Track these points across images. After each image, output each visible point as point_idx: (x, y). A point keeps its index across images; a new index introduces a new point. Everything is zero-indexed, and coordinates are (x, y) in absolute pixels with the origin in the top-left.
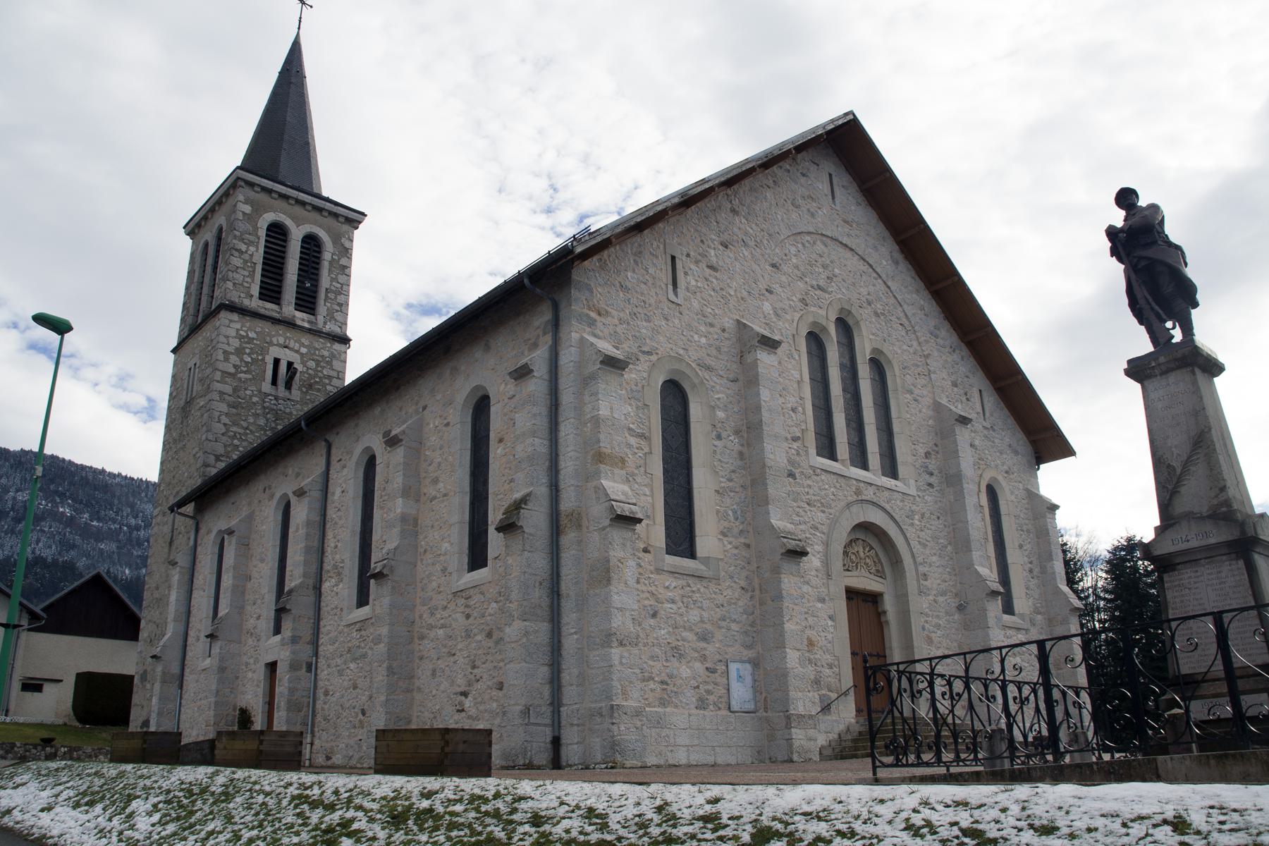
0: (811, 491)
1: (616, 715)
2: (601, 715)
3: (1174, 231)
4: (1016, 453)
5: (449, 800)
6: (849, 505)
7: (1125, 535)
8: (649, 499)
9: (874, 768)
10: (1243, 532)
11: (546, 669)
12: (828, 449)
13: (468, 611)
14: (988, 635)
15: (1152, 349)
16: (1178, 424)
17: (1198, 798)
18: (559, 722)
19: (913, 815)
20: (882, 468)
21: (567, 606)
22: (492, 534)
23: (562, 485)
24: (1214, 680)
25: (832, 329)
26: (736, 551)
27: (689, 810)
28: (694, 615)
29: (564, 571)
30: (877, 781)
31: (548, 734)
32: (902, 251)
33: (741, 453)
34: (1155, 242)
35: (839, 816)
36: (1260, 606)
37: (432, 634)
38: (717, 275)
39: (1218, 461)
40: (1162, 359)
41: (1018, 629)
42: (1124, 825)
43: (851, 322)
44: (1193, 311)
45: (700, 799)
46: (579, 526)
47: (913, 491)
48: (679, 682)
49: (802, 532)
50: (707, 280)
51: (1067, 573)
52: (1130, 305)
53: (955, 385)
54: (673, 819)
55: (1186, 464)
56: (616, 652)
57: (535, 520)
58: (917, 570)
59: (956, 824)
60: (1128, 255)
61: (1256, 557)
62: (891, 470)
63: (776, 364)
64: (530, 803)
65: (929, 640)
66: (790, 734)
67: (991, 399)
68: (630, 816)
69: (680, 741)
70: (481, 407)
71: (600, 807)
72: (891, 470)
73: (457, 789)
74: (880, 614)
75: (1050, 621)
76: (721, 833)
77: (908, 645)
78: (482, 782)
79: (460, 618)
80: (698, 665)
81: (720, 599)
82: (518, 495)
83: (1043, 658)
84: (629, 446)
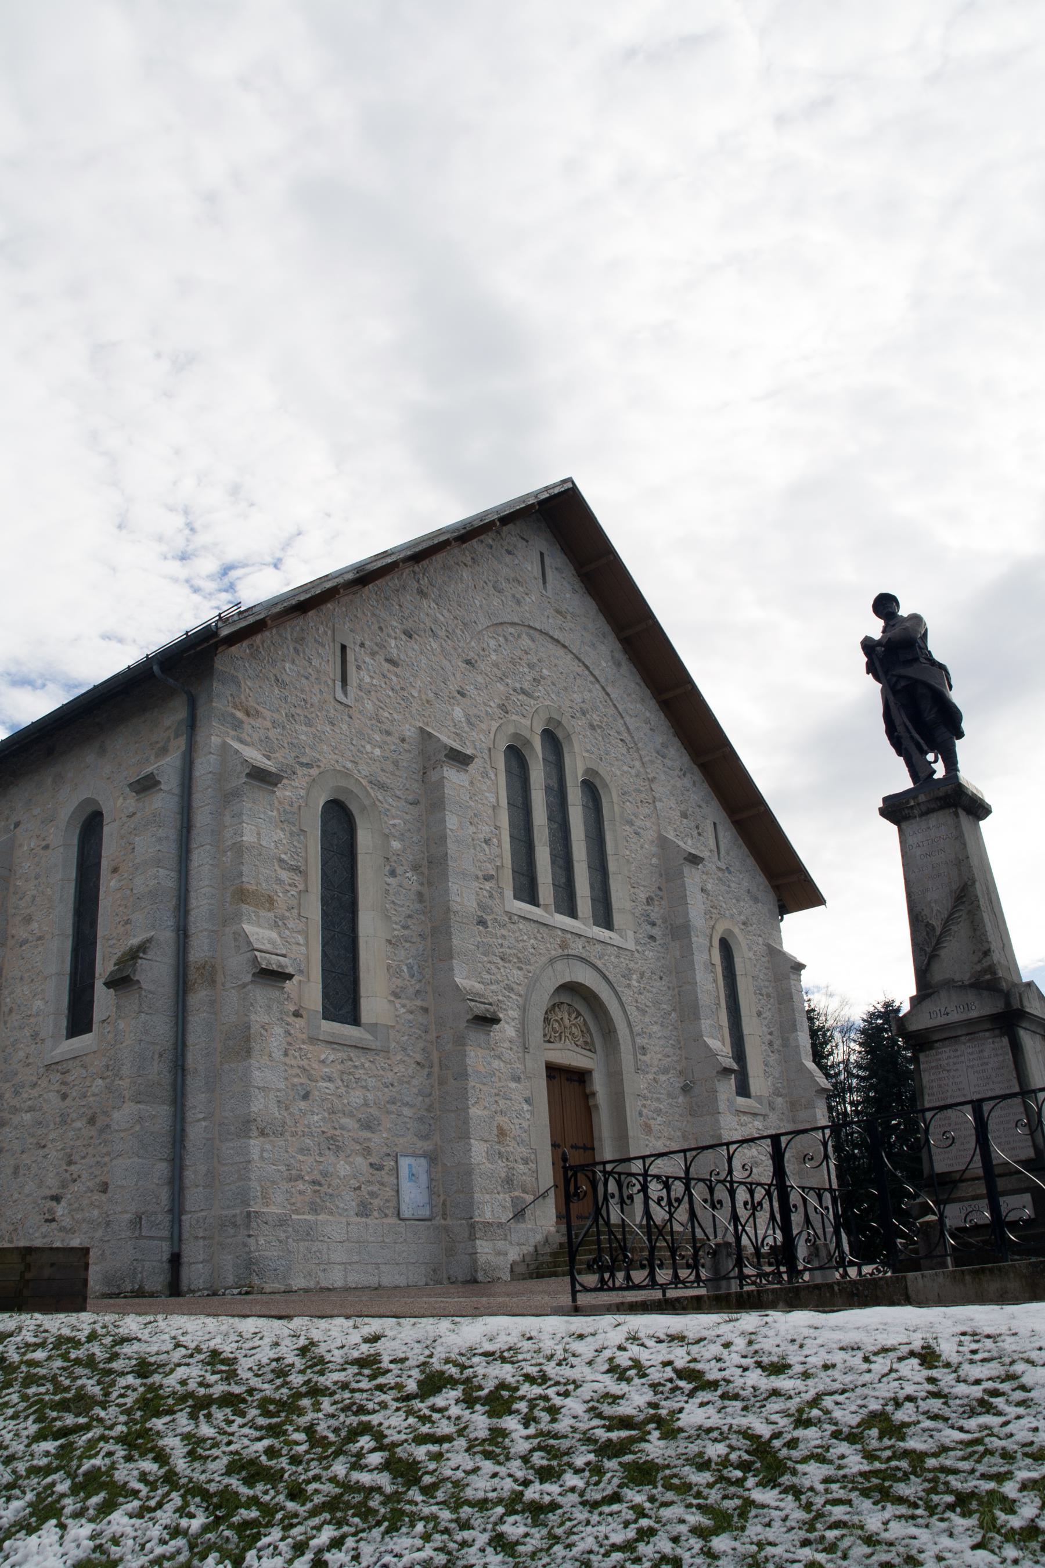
0: (506, 943)
1: (254, 1224)
2: (234, 1225)
3: (938, 647)
4: (756, 900)
5: (27, 1345)
6: (552, 961)
7: (882, 999)
8: (303, 949)
9: (574, 1293)
10: (1008, 1004)
12: (528, 891)
13: (64, 1089)
14: (717, 1121)
15: (907, 784)
16: (939, 875)
17: (949, 1323)
19: (619, 1353)
20: (594, 916)
21: (195, 1084)
23: (192, 929)
24: (973, 1179)
25: (537, 743)
26: (411, 1017)
27: (341, 1352)
28: (356, 1097)
29: (191, 1039)
30: (576, 1310)
31: (164, 1250)
33: (420, 895)
34: (916, 660)
35: (528, 1356)
36: (1026, 1092)
37: (16, 1119)
38: (398, 670)
39: (983, 921)
40: (922, 798)
41: (755, 1115)
42: (866, 1360)
43: (560, 735)
44: (957, 742)
45: (355, 1337)
46: (213, 982)
47: (631, 945)
48: (336, 1182)
50: (384, 676)
51: (814, 1046)
53: (684, 815)
54: (320, 1364)
56: (255, 1144)
57: (156, 973)
58: (634, 1042)
59: (670, 1363)
60: (886, 673)
61: (1022, 1033)
62: (605, 917)
63: (466, 784)
64: (136, 1346)
65: (648, 1129)
66: (474, 1247)
67: (728, 835)
68: (265, 1361)
69: (334, 1257)
70: (91, 825)
71: (227, 1349)
72: (605, 917)
73: (39, 1330)
74: (587, 1097)
75: (793, 1105)
76: (381, 1380)
77: (622, 1136)
78: (73, 1318)
79: (54, 1098)
80: (359, 1160)
81: (389, 1076)
82: (135, 941)
83: (778, 1157)
84: (279, 881)
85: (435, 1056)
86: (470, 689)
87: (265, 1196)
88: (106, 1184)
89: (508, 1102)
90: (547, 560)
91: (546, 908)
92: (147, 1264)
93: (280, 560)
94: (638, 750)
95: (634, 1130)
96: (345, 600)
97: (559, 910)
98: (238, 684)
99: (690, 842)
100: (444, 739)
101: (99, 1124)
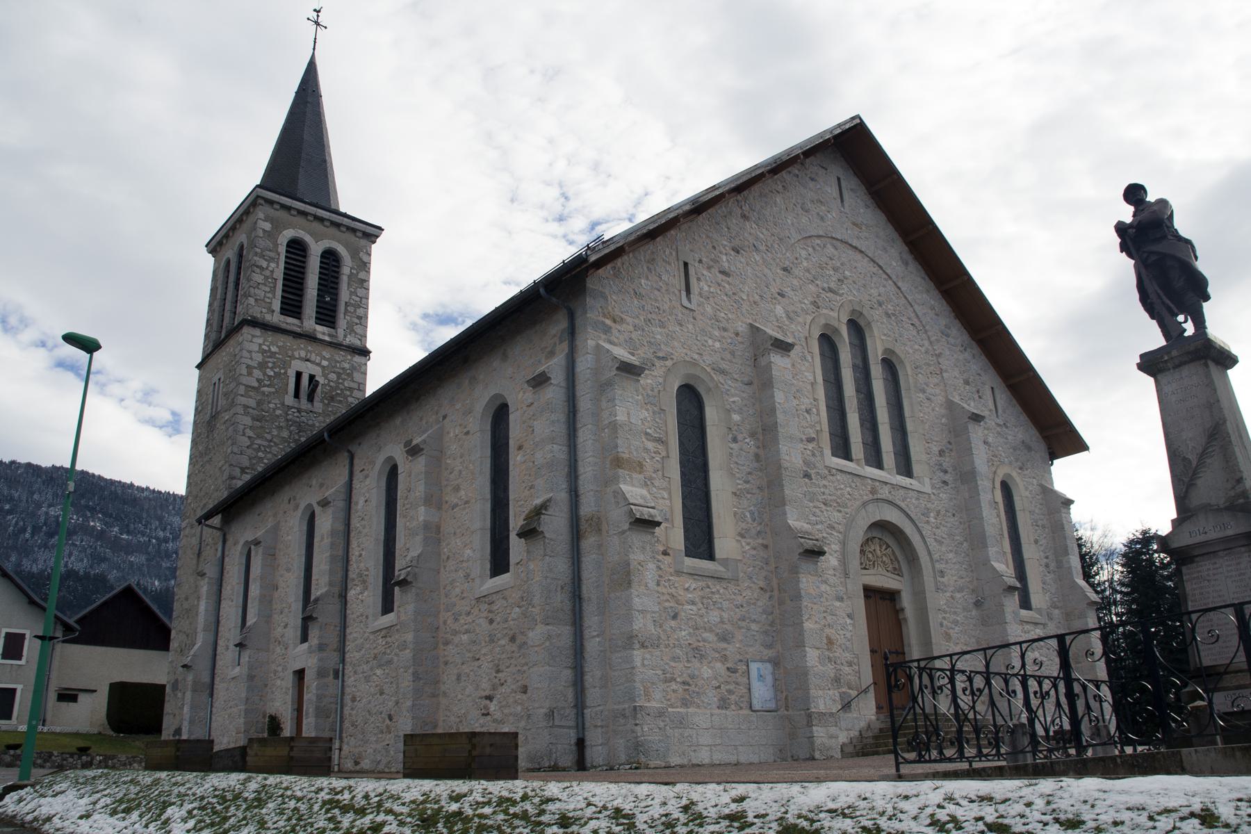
0: (827, 491)
1: (639, 716)
2: (624, 716)
3: (1182, 225)
5: (477, 803)
6: (864, 504)
7: (1140, 528)
12: (842, 448)
13: (491, 616)
14: (1005, 630)
15: (1162, 342)
17: (1225, 790)
18: (583, 724)
19: (938, 810)
20: (897, 467)
21: (589, 610)
23: (581, 490)
26: (754, 552)
28: (714, 616)
29: (585, 575)
30: (900, 778)
31: (572, 736)
32: (911, 252)
33: (757, 456)
34: (1164, 237)
35: (864, 813)
37: (456, 639)
38: (730, 279)
39: (1234, 453)
40: (1174, 353)
41: (1036, 624)
42: (1151, 818)
43: (862, 323)
44: (1205, 305)
45: (726, 798)
51: (1083, 567)
53: (967, 382)
55: (1203, 455)
57: (555, 525)
58: (933, 567)
59: (981, 819)
62: (906, 468)
63: (789, 366)
64: (558, 805)
65: (948, 637)
66: (811, 732)
67: (1003, 397)
68: (656, 816)
69: (702, 741)
70: (500, 415)
71: (627, 807)
72: (906, 468)
73: (485, 792)
74: (898, 612)
75: (1068, 616)
77: (927, 641)
78: (509, 784)
79: (484, 623)
80: (719, 665)
82: (538, 501)
83: (1063, 652)
84: (646, 450)
85: (775, 583)
86: (788, 290)
87: (647, 694)
90: (843, 184)
92: (559, 747)
94: (926, 332)
96: (685, 227)
97: (868, 464)
98: (605, 298)
100: (770, 331)
101: (518, 642)
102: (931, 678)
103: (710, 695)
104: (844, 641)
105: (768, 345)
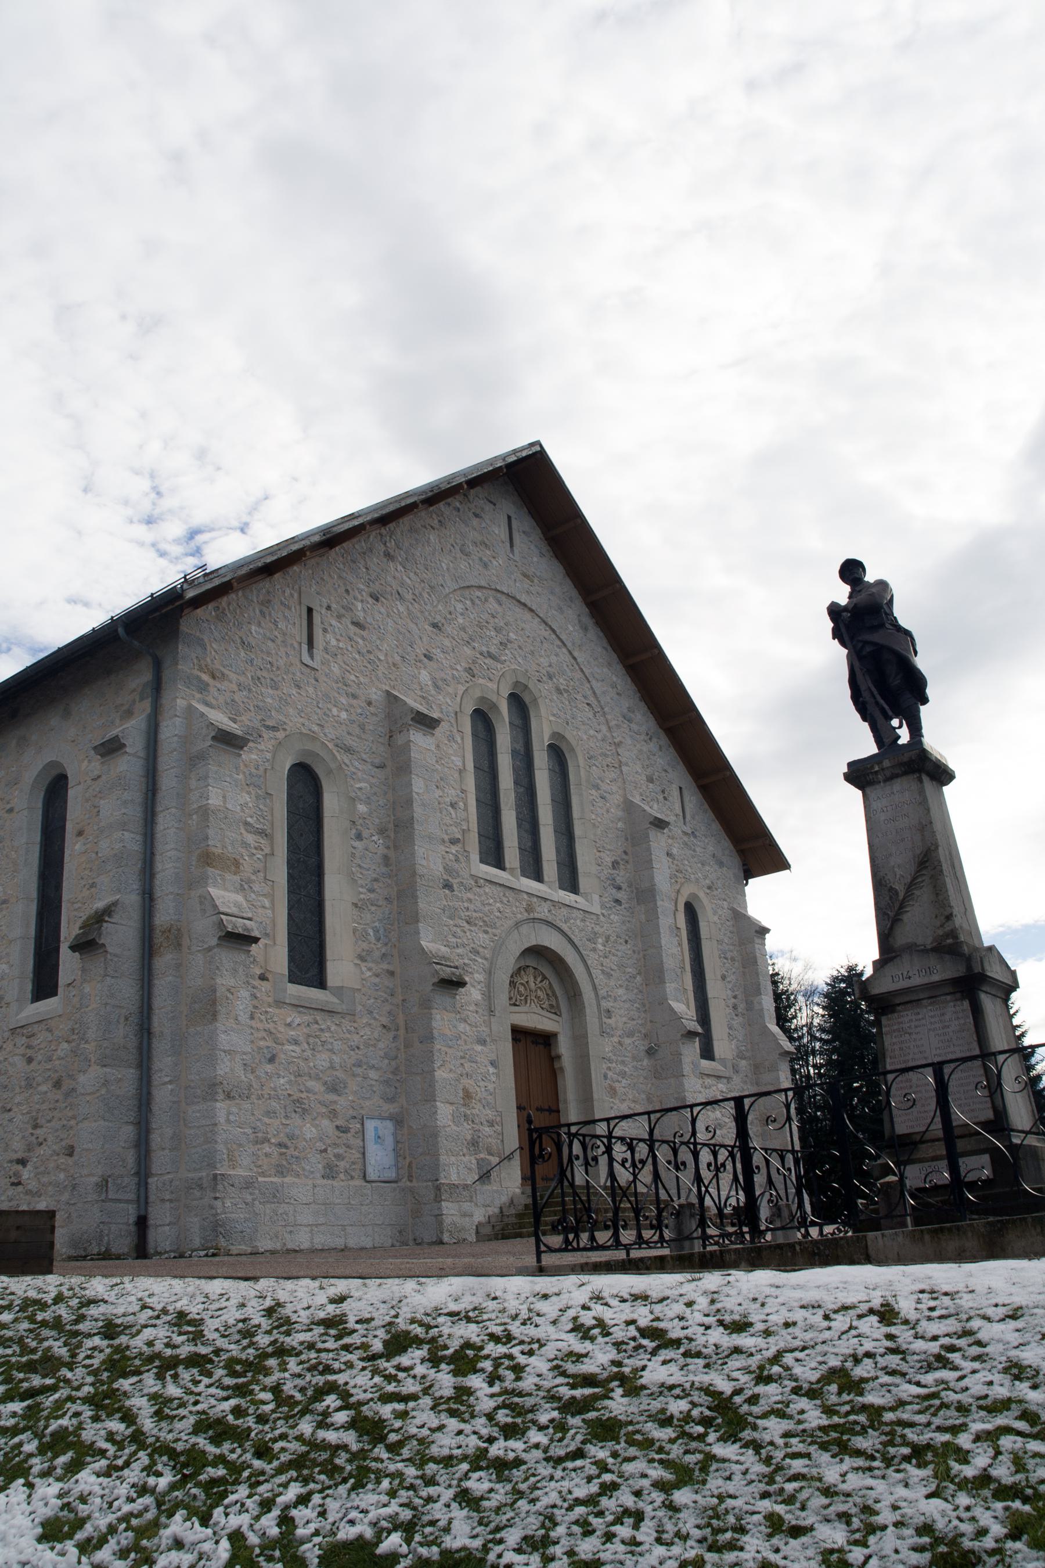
0: (472, 907)
1: (220, 1187)
2: (201, 1187)
3: (904, 613)
4: (721, 864)
6: (517, 925)
7: (846, 963)
9: (539, 1254)
10: (969, 968)
11: (130, 1128)
12: (494, 855)
13: (29, 1052)
14: (682, 1084)
15: (875, 750)
17: (908, 1281)
18: (147, 1198)
19: (583, 1312)
20: (560, 879)
21: (161, 1049)
22: (65, 953)
23: (158, 893)
25: (504, 707)
26: (377, 980)
27: (307, 1312)
28: (322, 1060)
29: (157, 1002)
30: (541, 1271)
31: (131, 1213)
32: (593, 615)
33: (386, 858)
34: (882, 625)
35: (493, 1316)
39: (944, 884)
40: (886, 763)
41: (719, 1077)
42: (826, 1317)
43: (527, 699)
44: (922, 708)
45: (321, 1298)
47: (596, 909)
49: (459, 956)
50: (351, 639)
52: (852, 697)
53: (650, 780)
54: (286, 1325)
55: (911, 886)
56: (221, 1107)
57: (121, 936)
58: (599, 1005)
59: (633, 1322)
60: (852, 639)
62: (570, 881)
63: (433, 748)
64: (103, 1308)
65: (613, 1091)
66: (440, 1208)
67: (693, 799)
68: (231, 1322)
70: (56, 789)
71: (194, 1310)
72: (570, 881)
74: (553, 1059)
76: (347, 1340)
78: (39, 1281)
79: (19, 1062)
80: (325, 1122)
82: (100, 905)
83: (741, 1119)
84: (245, 845)
86: (437, 653)
88: (72, 1147)
89: (473, 1065)
90: (515, 524)
91: (512, 871)
92: (113, 1227)
93: (247, 524)
95: (599, 1092)
97: (524, 875)
99: (655, 806)
100: (410, 702)
102: (584, 1145)
103: (313, 1160)
104: (485, 1094)
105: (408, 720)
